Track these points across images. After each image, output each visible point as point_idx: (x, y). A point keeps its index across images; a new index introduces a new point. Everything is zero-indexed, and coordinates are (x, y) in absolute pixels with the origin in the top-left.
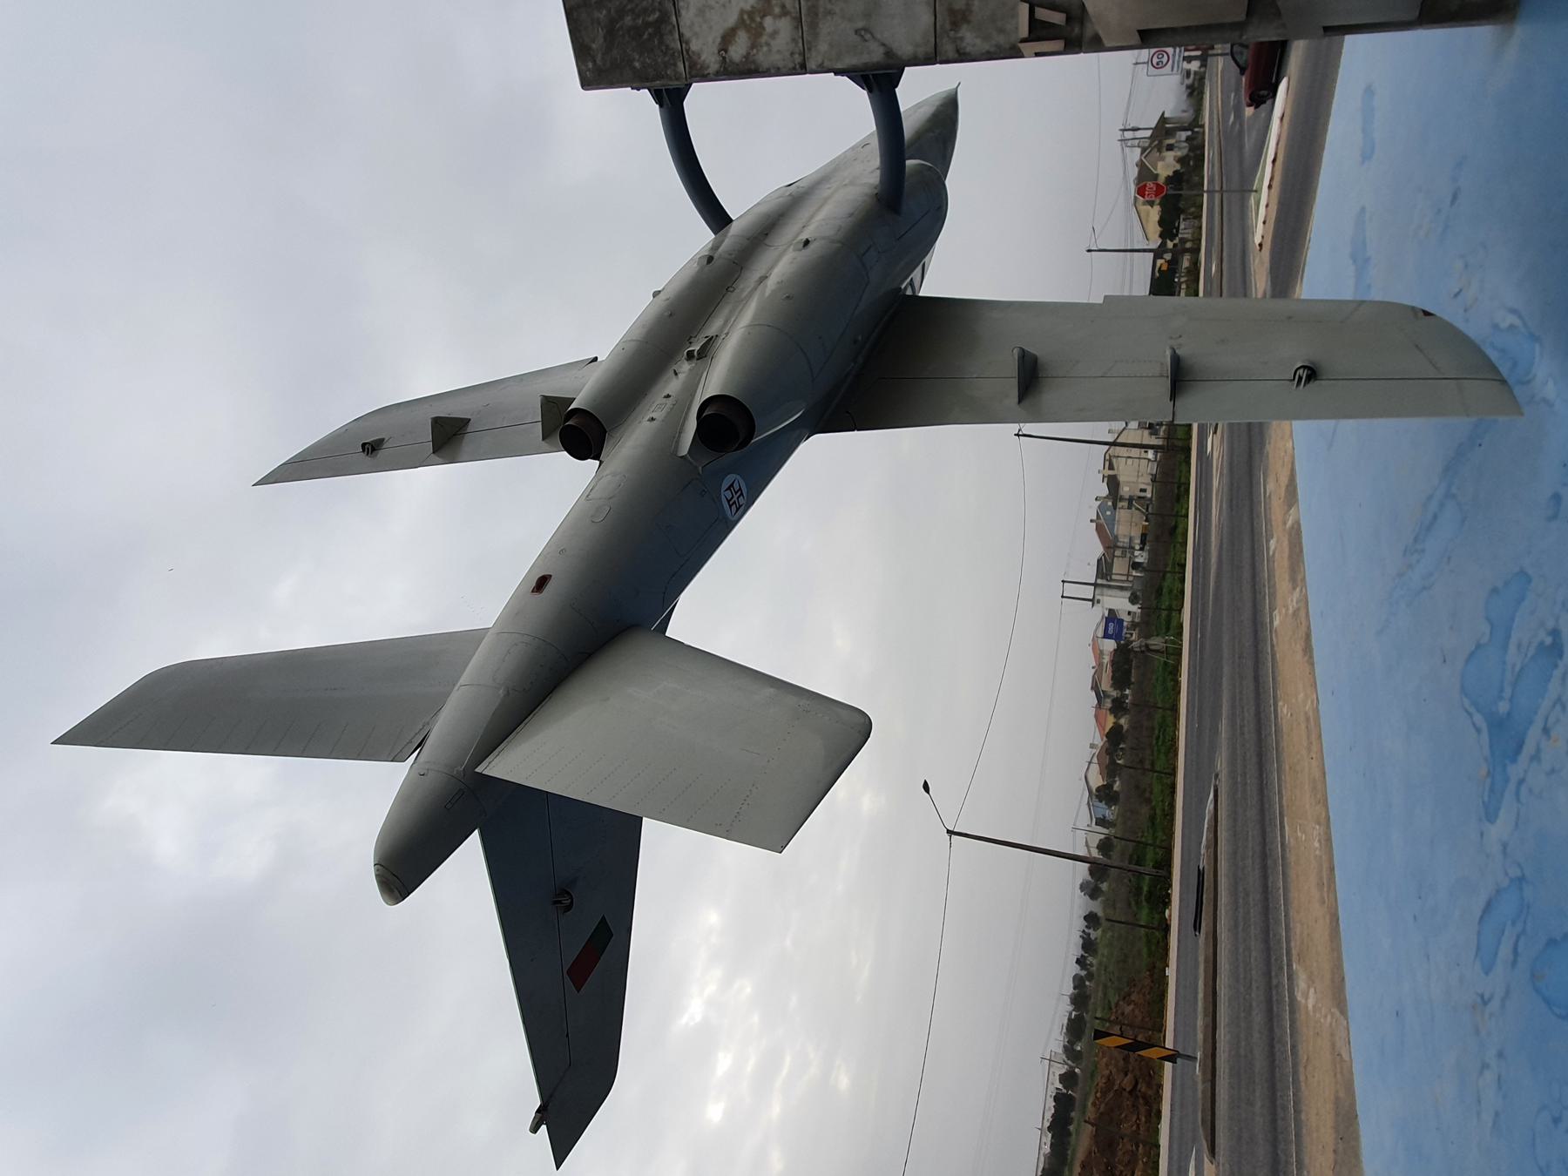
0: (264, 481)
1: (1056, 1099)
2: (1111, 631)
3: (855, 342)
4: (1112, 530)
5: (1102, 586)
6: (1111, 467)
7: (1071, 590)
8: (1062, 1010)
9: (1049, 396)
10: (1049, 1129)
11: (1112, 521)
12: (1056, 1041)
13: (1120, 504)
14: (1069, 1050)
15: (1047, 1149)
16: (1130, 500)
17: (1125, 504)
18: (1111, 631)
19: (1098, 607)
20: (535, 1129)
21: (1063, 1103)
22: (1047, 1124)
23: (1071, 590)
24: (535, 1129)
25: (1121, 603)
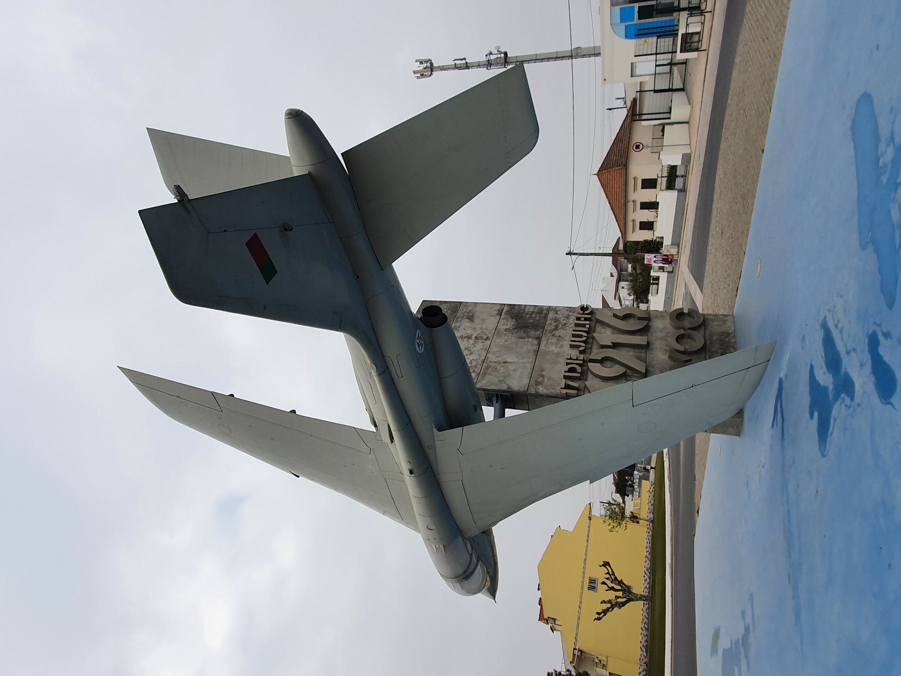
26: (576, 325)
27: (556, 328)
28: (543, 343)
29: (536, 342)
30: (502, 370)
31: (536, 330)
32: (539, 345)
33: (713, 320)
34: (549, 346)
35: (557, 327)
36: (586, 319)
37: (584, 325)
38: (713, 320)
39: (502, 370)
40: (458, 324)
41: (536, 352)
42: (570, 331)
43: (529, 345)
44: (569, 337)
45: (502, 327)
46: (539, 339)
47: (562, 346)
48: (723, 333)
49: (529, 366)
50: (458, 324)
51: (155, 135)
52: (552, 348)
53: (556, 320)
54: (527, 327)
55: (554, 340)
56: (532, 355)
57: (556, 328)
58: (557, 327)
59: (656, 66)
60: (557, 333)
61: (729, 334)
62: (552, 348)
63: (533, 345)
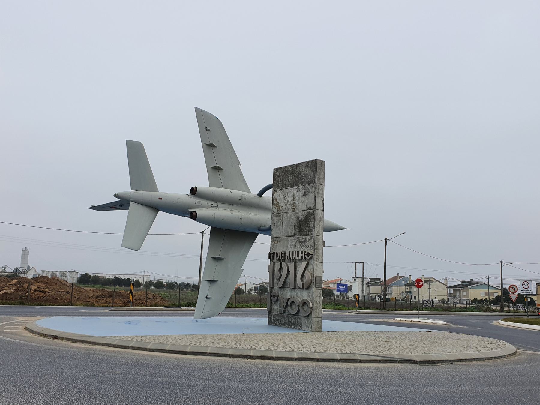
0: (94, 208)
1: (129, 279)
2: (341, 287)
3: (5, 268)
4: (394, 284)
5: (363, 281)
6: (426, 282)
7: (360, 266)
8: (167, 279)
9: (213, 263)
10: (115, 277)
11: (399, 284)
12: (154, 277)
13: (408, 287)
14: (151, 283)
15: (107, 277)
16: (410, 292)
17: (408, 290)
18: (341, 287)
19: (352, 280)
20: (116, 196)
21: (127, 282)
22: (117, 276)
23: (360, 266)
24: (116, 196)
25: (357, 289)
26: (298, 252)
27: (301, 242)
28: (292, 238)
29: (293, 234)
30: (279, 223)
31: (299, 232)
32: (291, 236)
33: (308, 321)
34: (291, 241)
35: (301, 242)
36: (302, 257)
37: (298, 256)
38: (308, 321)
39: (279, 223)
40: (301, 189)
41: (288, 236)
42: (299, 250)
43: (291, 231)
44: (296, 250)
45: (300, 214)
46: (295, 235)
47: (291, 247)
48: (301, 324)
49: (281, 235)
50: (301, 189)
51: (200, 113)
52: (290, 243)
53: (305, 241)
54: (300, 227)
55: (294, 243)
56: (286, 234)
57: (301, 242)
58: (301, 242)
59: (356, 263)
60: (298, 244)
61: (301, 327)
62: (290, 243)
63: (291, 233)
